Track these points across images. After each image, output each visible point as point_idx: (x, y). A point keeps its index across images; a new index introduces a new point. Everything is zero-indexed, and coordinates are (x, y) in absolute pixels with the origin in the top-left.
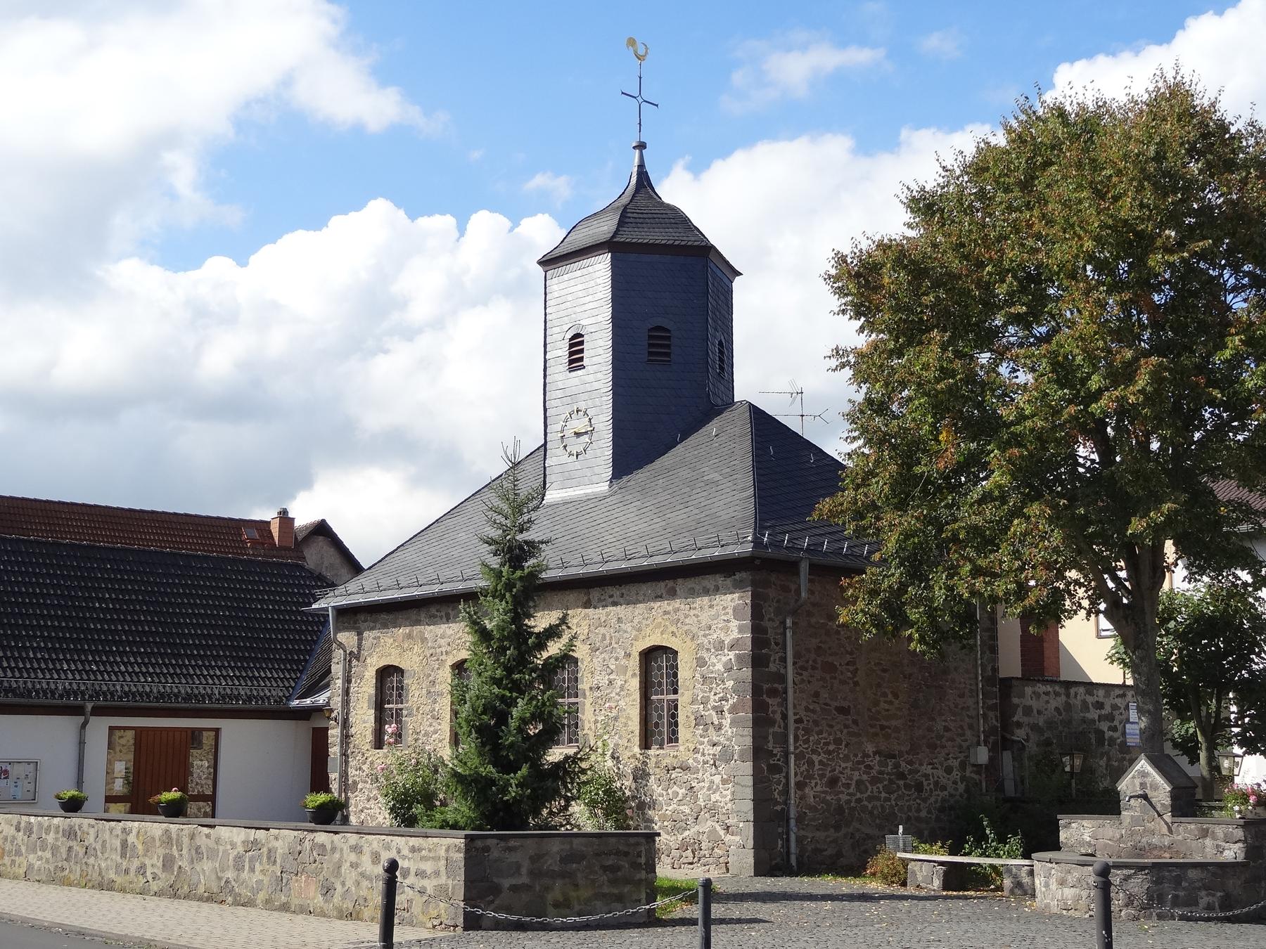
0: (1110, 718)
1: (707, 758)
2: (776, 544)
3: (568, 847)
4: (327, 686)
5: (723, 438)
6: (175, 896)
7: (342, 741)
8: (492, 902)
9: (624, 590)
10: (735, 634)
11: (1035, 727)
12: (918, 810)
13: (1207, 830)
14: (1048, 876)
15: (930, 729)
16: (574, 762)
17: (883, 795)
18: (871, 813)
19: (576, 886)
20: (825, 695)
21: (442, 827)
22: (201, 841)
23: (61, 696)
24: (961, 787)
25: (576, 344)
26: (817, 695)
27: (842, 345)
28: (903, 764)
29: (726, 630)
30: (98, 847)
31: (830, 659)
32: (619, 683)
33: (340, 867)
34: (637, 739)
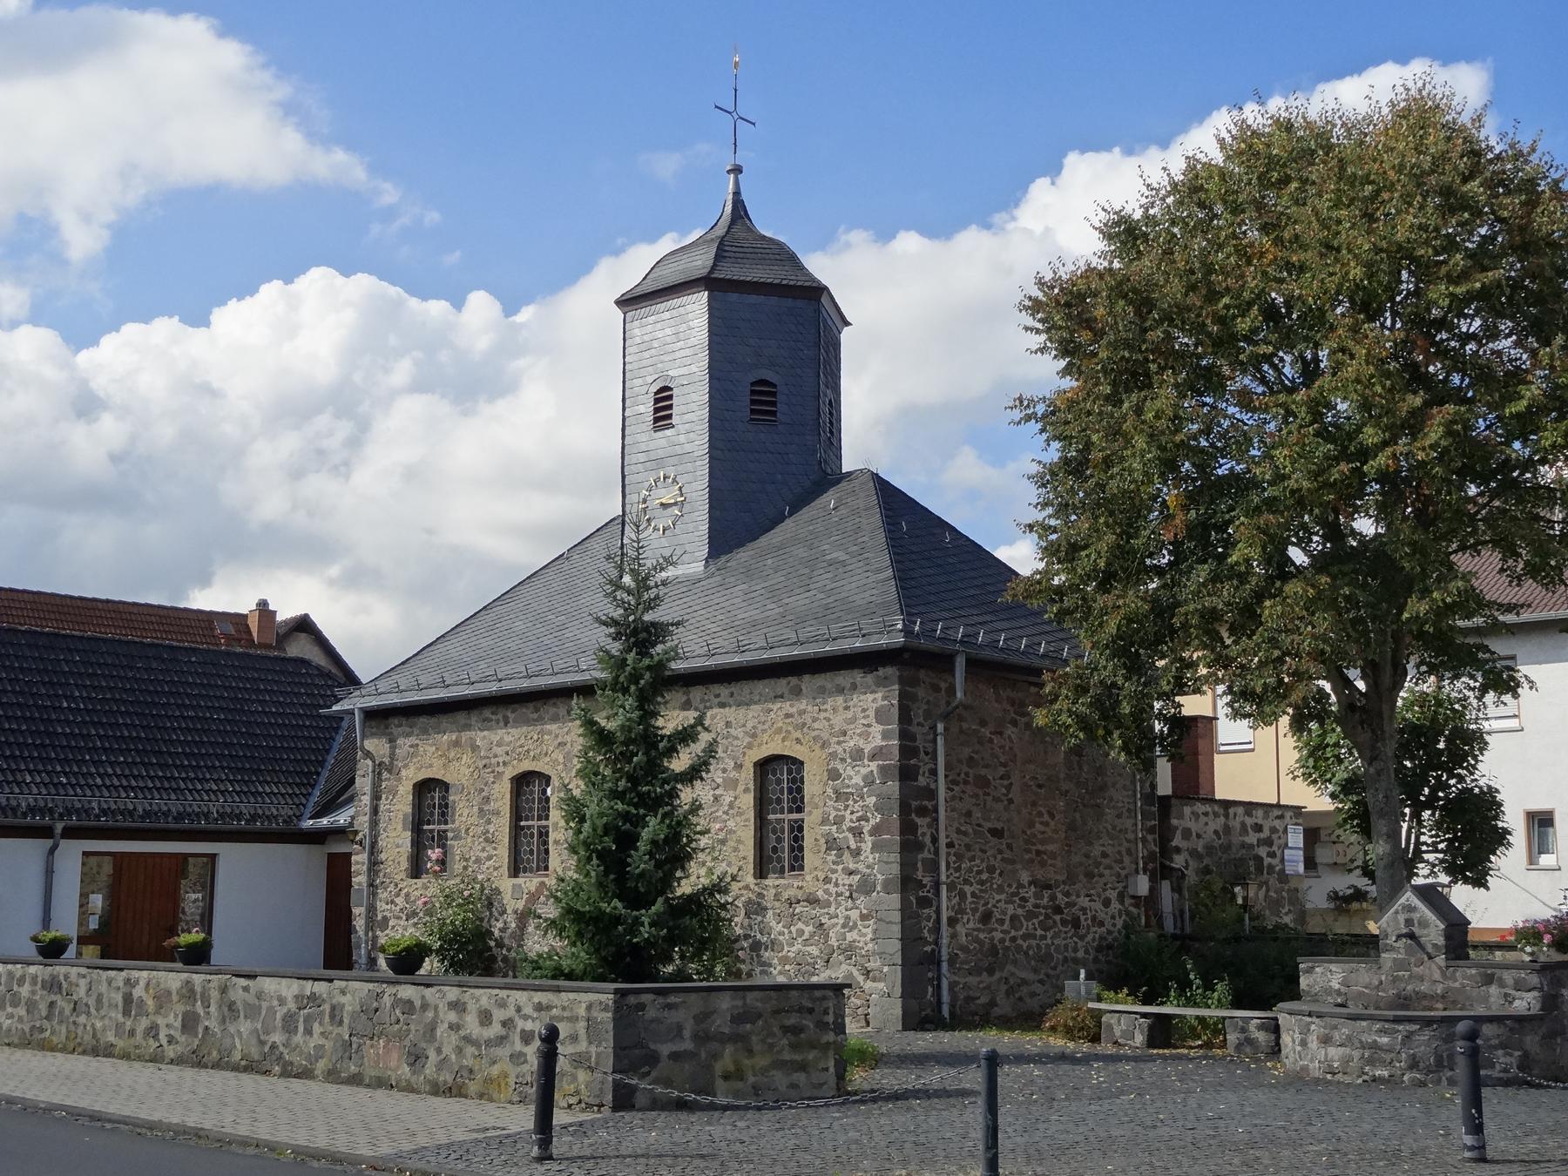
0: (1268, 842)
1: (841, 889)
2: (928, 633)
4: (351, 799)
5: (843, 511)
6: (200, 1064)
7: (369, 870)
8: (648, 1073)
9: (735, 688)
10: (878, 741)
11: (1194, 853)
12: (1075, 950)
13: (1493, 975)
14: (1305, 1031)
15: (1087, 856)
16: (711, 895)
17: (1039, 932)
18: (1026, 953)
20: (977, 814)
21: (554, 977)
22: (237, 995)
23: (25, 815)
24: (1119, 923)
25: (663, 403)
26: (969, 814)
27: (1027, 395)
28: (1059, 896)
29: (866, 735)
30: (92, 1002)
31: (983, 772)
32: (728, 799)
33: (433, 1030)
34: (751, 866)
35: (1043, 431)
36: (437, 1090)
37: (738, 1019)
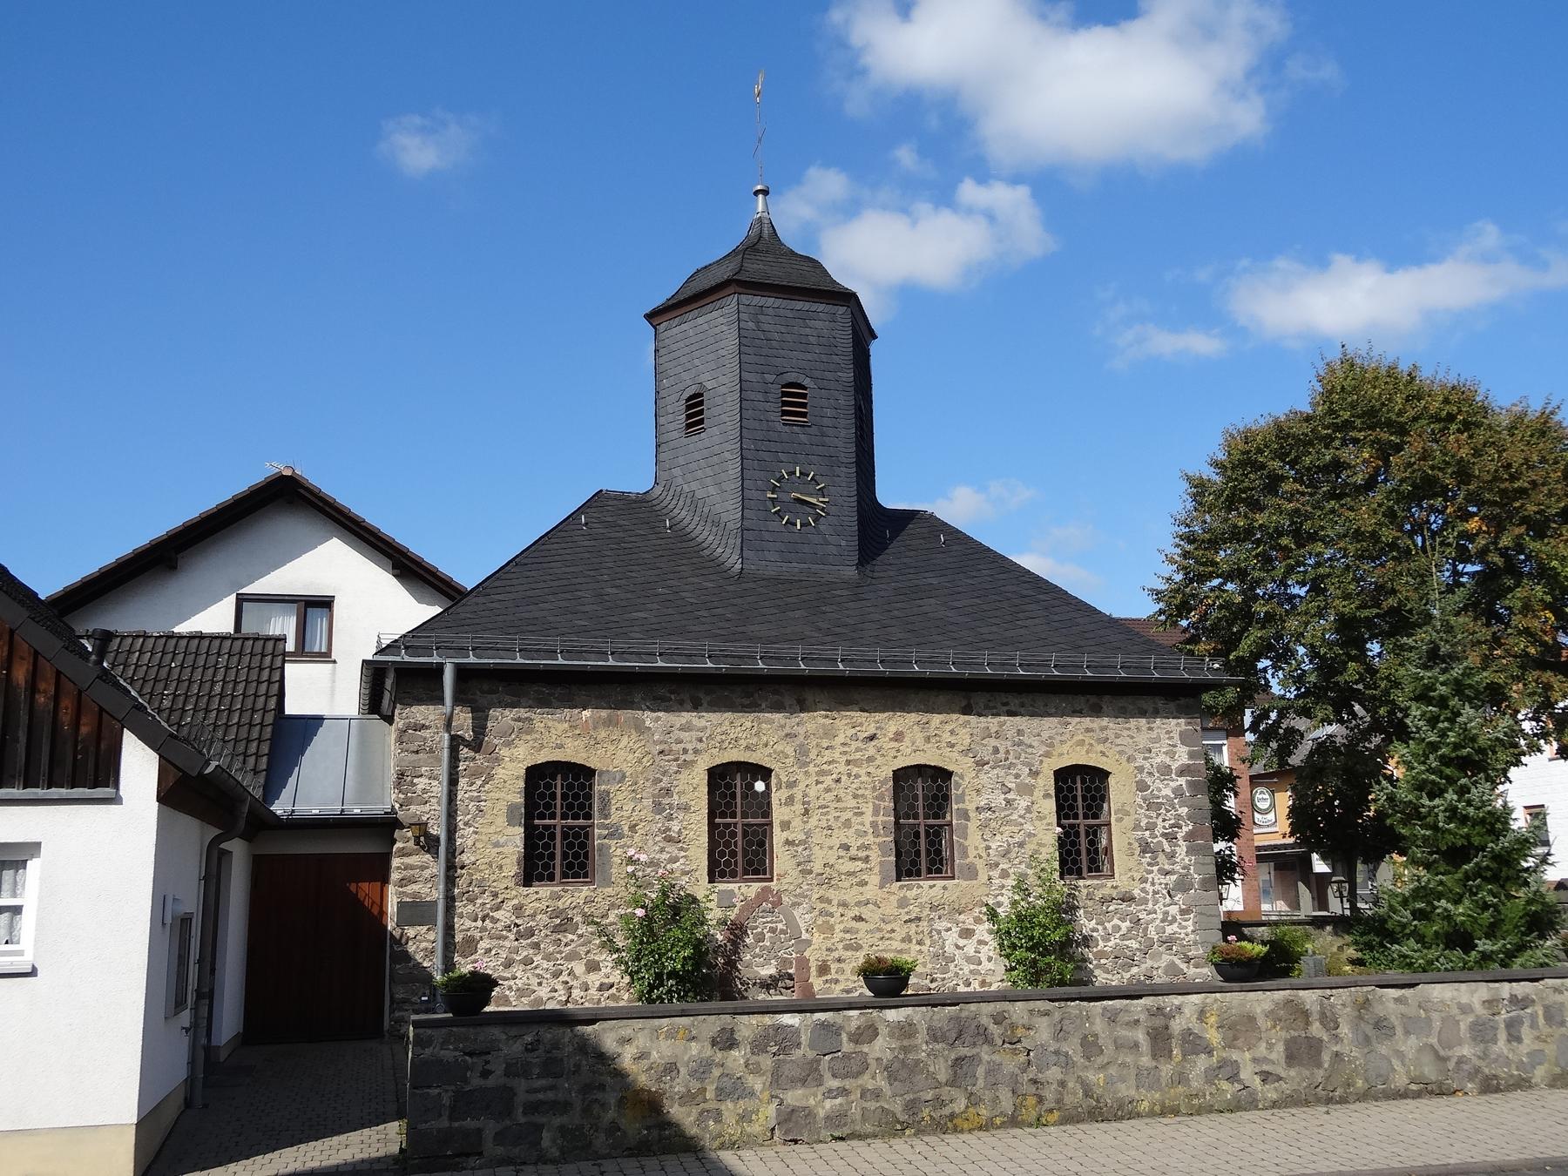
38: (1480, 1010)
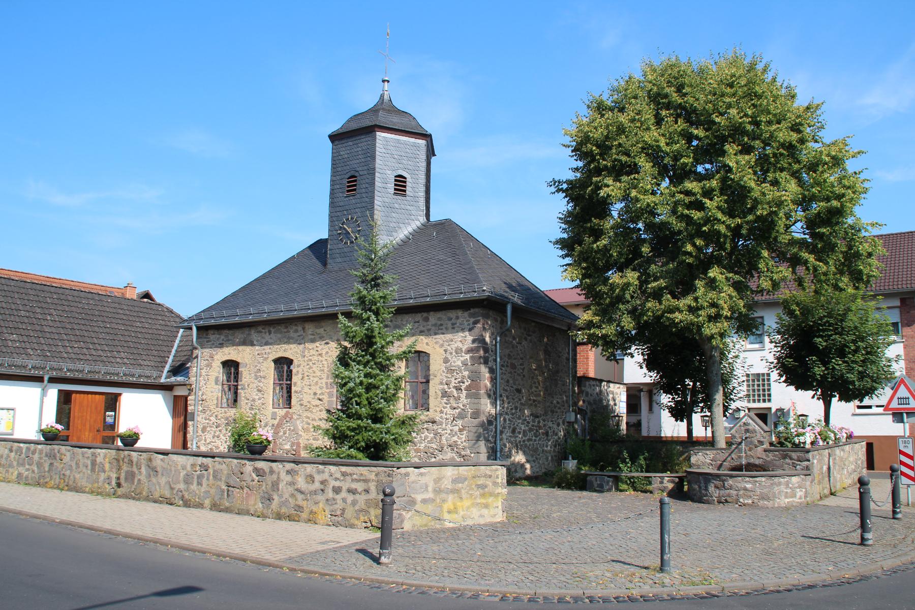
1: (448, 416)
3: (456, 472)
19: (461, 498)
20: (511, 382)
26: (508, 381)
31: (514, 361)
35: (566, 197)
36: (279, 517)
37: (455, 481)
38: (189, 468)
